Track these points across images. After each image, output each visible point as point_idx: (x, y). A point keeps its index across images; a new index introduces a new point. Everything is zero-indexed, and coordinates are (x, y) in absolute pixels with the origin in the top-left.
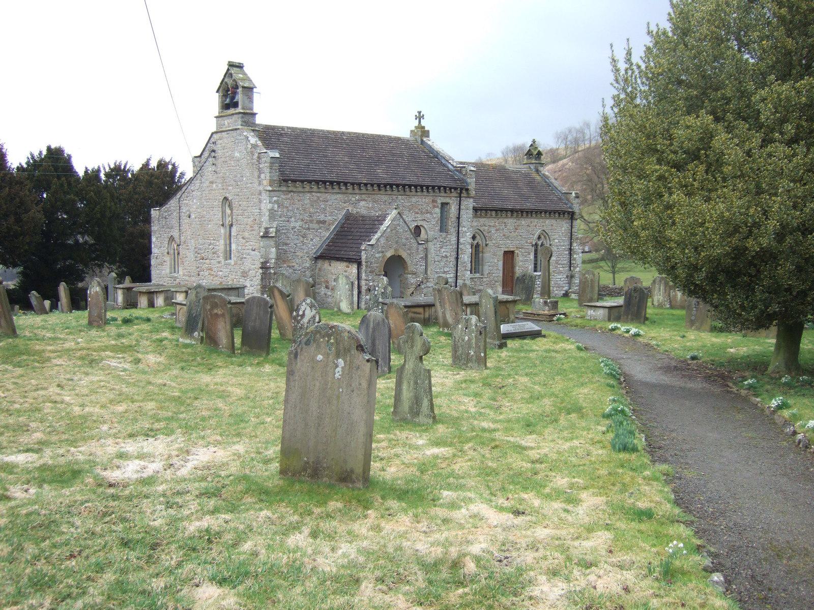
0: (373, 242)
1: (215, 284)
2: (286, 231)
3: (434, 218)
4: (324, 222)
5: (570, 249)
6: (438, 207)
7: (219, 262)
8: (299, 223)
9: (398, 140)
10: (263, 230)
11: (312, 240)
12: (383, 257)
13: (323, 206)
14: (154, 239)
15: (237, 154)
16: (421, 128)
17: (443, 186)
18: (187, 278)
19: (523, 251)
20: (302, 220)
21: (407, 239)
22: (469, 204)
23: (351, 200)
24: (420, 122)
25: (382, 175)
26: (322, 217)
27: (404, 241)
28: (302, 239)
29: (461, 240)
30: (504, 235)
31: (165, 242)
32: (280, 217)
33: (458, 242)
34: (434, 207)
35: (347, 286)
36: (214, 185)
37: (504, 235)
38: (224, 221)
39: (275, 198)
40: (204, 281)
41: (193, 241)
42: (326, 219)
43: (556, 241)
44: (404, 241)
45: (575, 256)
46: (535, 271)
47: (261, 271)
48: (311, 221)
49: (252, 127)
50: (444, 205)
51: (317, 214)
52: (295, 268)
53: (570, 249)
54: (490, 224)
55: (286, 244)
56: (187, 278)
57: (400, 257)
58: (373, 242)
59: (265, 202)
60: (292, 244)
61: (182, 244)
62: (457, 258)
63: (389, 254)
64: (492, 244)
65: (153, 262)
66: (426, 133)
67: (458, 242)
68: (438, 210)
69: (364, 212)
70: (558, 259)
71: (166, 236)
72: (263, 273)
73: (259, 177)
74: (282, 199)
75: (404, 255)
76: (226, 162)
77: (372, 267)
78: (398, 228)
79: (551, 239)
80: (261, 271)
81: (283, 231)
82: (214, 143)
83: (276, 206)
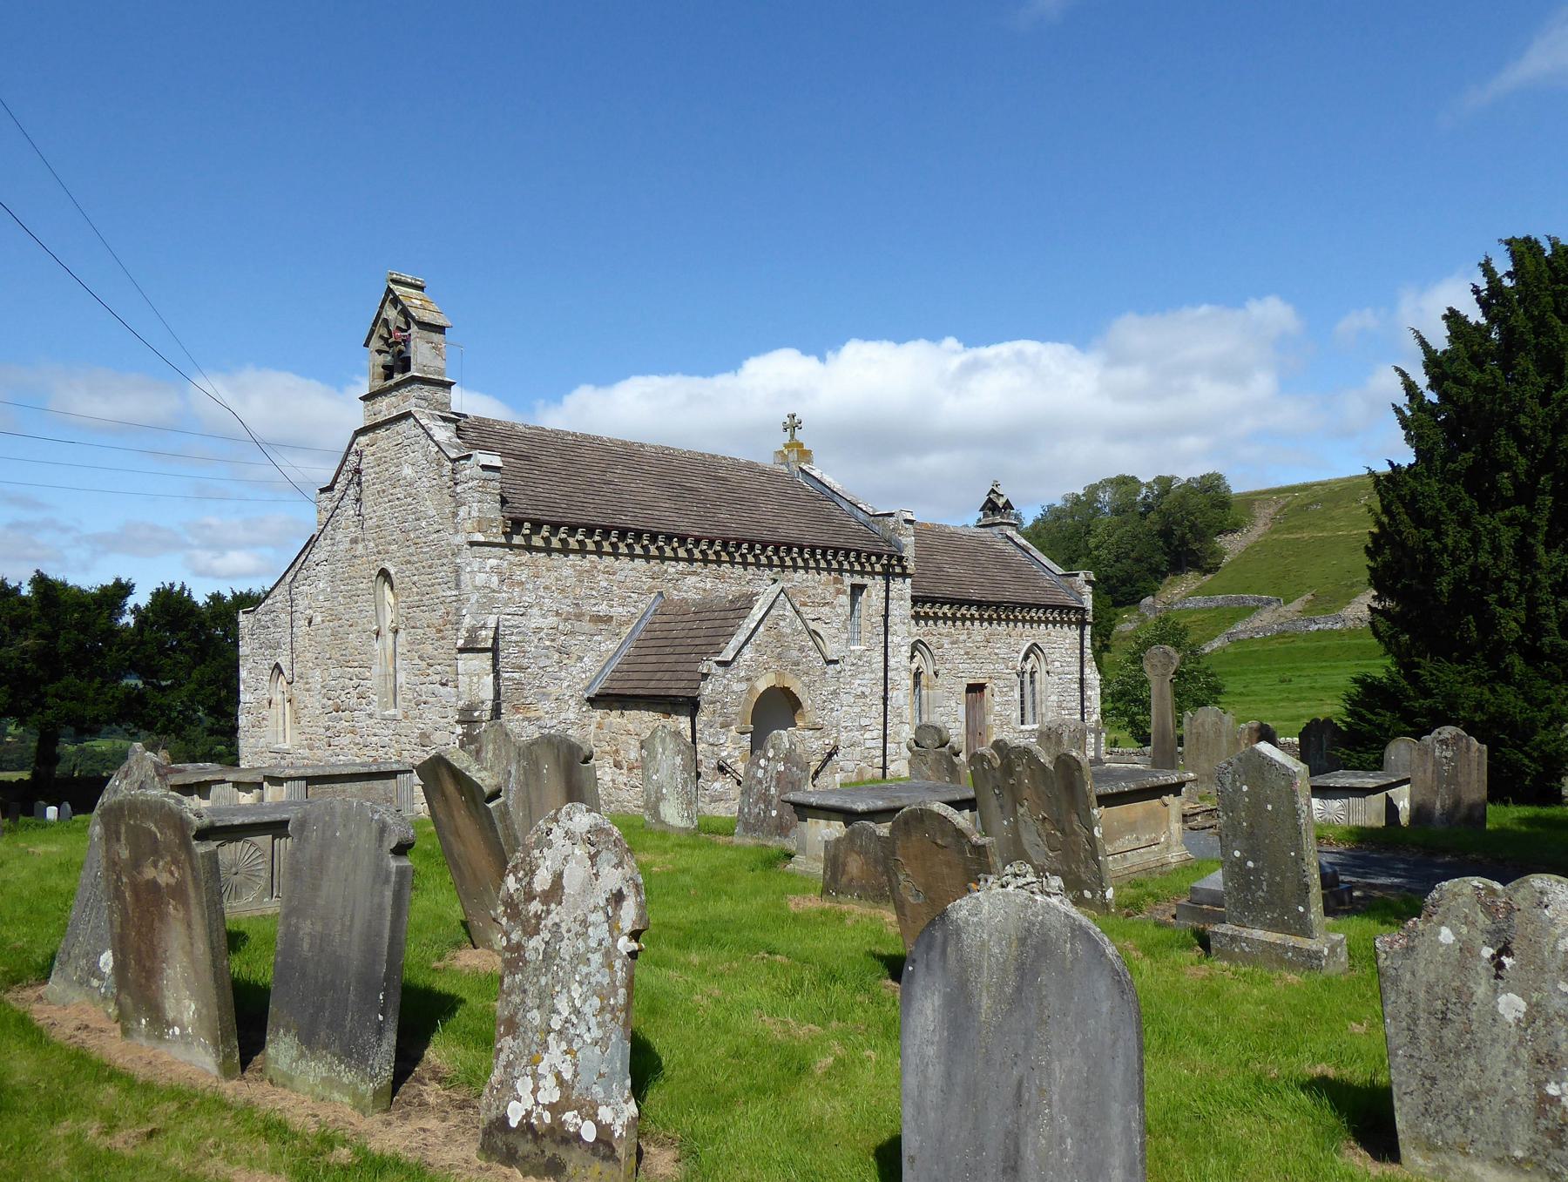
0: (728, 655)
1: (363, 765)
2: (519, 639)
3: (839, 615)
4: (608, 619)
5: (1082, 680)
6: (844, 592)
7: (370, 716)
8: (552, 620)
9: (751, 466)
10: (463, 633)
11: (580, 659)
12: (751, 690)
13: (604, 584)
14: (243, 674)
15: (408, 471)
16: (794, 445)
17: (854, 550)
18: (306, 752)
19: (1001, 683)
20: (557, 614)
21: (801, 649)
22: (903, 589)
23: (666, 571)
24: (792, 436)
25: (731, 521)
26: (603, 609)
27: (795, 653)
28: (556, 656)
29: (892, 662)
30: (967, 653)
31: (265, 678)
32: (506, 605)
33: (886, 666)
34: (839, 592)
35: (678, 760)
36: (360, 546)
37: (967, 653)
38: (381, 624)
39: (493, 562)
40: (341, 757)
41: (318, 672)
42: (614, 612)
43: (1057, 664)
44: (795, 653)
45: (1089, 693)
46: (1022, 723)
47: (459, 730)
48: (579, 617)
49: (442, 412)
50: (857, 590)
51: (593, 601)
52: (541, 723)
53: (1082, 680)
54: (940, 634)
55: (521, 668)
56: (306, 752)
57: (786, 693)
58: (728, 655)
59: (468, 569)
60: (533, 669)
61: (296, 679)
62: (885, 699)
63: (762, 685)
64: (946, 671)
65: (243, 721)
66: (805, 455)
67: (886, 666)
68: (845, 599)
69: (693, 595)
70: (1062, 698)
71: (266, 667)
72: (464, 735)
73: (455, 515)
74: (511, 563)
75: (797, 688)
76: (384, 491)
77: (725, 715)
78: (782, 623)
79: (1049, 660)
80: (459, 730)
81: (514, 638)
82: (360, 454)
83: (495, 579)
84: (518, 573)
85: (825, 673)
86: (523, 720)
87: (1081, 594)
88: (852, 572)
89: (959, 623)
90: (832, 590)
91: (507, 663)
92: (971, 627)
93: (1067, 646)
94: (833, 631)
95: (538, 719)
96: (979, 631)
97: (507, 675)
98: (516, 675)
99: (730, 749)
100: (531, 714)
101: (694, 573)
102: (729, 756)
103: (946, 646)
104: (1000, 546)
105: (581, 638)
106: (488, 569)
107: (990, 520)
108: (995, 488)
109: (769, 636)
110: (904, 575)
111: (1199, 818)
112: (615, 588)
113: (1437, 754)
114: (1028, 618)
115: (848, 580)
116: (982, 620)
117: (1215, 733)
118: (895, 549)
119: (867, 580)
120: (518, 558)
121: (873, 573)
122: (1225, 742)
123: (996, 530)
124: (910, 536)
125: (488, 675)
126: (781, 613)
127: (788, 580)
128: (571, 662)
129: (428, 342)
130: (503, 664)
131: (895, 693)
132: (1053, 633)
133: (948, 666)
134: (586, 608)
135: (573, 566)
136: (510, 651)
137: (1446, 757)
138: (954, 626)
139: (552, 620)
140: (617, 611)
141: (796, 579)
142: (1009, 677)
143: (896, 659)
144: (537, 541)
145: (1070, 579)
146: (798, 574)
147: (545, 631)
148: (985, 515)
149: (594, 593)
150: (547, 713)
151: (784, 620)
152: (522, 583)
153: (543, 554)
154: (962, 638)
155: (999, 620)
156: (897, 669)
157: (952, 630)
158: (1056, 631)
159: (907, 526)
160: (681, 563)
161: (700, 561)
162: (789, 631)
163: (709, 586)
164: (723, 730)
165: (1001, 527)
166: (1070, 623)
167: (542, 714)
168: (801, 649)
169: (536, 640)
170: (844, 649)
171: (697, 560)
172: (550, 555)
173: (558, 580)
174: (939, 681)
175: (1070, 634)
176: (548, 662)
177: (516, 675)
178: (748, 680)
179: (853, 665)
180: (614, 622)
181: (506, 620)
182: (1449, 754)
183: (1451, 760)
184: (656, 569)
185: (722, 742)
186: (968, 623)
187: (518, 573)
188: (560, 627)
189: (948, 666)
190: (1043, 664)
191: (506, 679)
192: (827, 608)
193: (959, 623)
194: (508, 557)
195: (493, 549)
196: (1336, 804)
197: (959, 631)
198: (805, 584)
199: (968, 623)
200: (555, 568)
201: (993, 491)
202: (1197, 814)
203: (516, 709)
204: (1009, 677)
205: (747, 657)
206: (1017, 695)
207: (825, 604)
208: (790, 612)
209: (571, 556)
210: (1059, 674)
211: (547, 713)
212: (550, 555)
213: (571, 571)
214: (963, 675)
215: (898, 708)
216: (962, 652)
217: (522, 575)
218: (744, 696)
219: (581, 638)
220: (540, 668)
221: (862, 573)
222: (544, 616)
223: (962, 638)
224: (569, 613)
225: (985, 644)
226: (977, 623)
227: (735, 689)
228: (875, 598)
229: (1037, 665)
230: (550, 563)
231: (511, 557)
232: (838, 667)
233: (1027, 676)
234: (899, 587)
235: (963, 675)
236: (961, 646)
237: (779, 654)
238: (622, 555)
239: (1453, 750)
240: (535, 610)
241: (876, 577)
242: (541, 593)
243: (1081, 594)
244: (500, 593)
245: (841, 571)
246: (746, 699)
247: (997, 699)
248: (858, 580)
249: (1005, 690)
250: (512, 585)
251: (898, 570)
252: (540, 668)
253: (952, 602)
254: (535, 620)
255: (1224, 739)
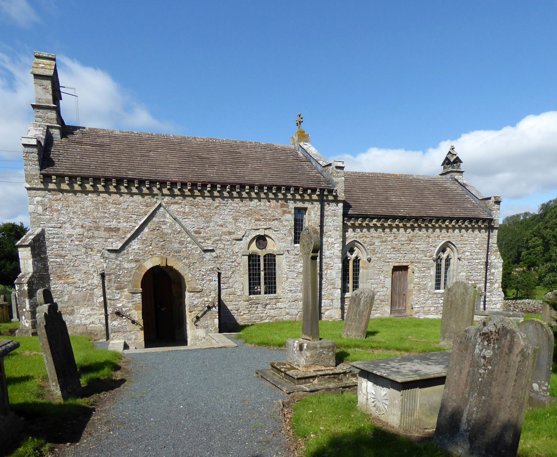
2: (58, 240)
3: (285, 226)
6: (290, 212)
8: (79, 230)
12: (139, 268)
13: (113, 210)
19: (420, 265)
20: (82, 227)
21: (181, 243)
26: (114, 224)
27: (176, 246)
28: (83, 250)
30: (394, 248)
34: (284, 212)
48: (97, 228)
49: (51, 123)
52: (77, 285)
53: (487, 263)
55: (61, 256)
63: (149, 265)
70: (469, 274)
74: (50, 199)
78: (163, 227)
81: (55, 240)
84: (56, 205)
85: (203, 258)
86: (64, 283)
87: (491, 210)
88: (295, 200)
89: (387, 230)
90: (280, 211)
91: (52, 253)
92: (397, 232)
93: (477, 243)
94: (280, 235)
95: (74, 283)
96: (403, 235)
97: (52, 260)
98: (58, 260)
99: (124, 302)
100: (70, 281)
101: (176, 203)
102: (123, 306)
103: (376, 244)
104: (448, 185)
105: (99, 240)
106: (35, 203)
107: (446, 171)
108: (451, 151)
109: (153, 234)
110: (336, 200)
111: (316, 381)
112: (121, 212)
113: (477, 351)
114: (457, 226)
115: (292, 205)
116: (405, 228)
117: (462, 301)
118: (331, 185)
119: (307, 205)
120: (55, 197)
121: (311, 201)
122: (467, 308)
123: (448, 176)
124: (341, 177)
125: (30, 259)
126: (162, 220)
127: (246, 206)
128: (94, 253)
129: (40, 86)
130: (49, 254)
131: (329, 271)
132: (465, 235)
133: (378, 255)
134: (101, 224)
135: (92, 200)
136: (53, 247)
137: (484, 357)
138: (384, 231)
139: (79, 230)
140: (123, 225)
141: (251, 205)
142: (427, 261)
143: (330, 252)
144: (64, 186)
145: (487, 201)
146: (253, 202)
147: (75, 236)
148: (445, 168)
149: (106, 215)
150: (80, 280)
151: (165, 224)
152: (58, 210)
153: (71, 194)
154: (389, 239)
155: (420, 228)
156: (331, 257)
157: (382, 234)
158: (468, 235)
159: (338, 170)
160: (167, 198)
161: (180, 195)
162: (170, 231)
163: (187, 210)
164: (117, 291)
165: (451, 174)
166: (480, 228)
167: (76, 280)
168: (181, 243)
169: (69, 241)
170: (289, 245)
171: (177, 195)
172: (75, 194)
173: (81, 208)
174: (371, 264)
175: (479, 235)
176: (78, 253)
177: (58, 260)
178: (136, 261)
179: (296, 255)
180: (121, 231)
181: (49, 230)
182: (488, 353)
183: (489, 361)
184: (149, 201)
185: (117, 298)
186: (395, 230)
187: (56, 205)
188: (85, 234)
189: (378, 255)
190: (456, 254)
191: (52, 262)
192: (276, 222)
193: (387, 230)
194: (48, 196)
195: (38, 192)
196: (384, 391)
197: (388, 235)
198: (258, 208)
199: (395, 230)
200: (80, 202)
201: (450, 153)
202: (314, 377)
203: (60, 278)
204: (427, 261)
205: (136, 247)
206: (433, 272)
207: (274, 220)
208: (169, 219)
209: (90, 195)
210: (468, 259)
211: (80, 280)
212: (75, 194)
213: (89, 203)
214: (390, 260)
215: (331, 280)
216: (390, 247)
217: (58, 206)
218: (134, 271)
219: (99, 240)
220: (74, 256)
221: (303, 200)
222: (73, 228)
223: (389, 239)
224: (90, 226)
225: (409, 242)
226: (402, 230)
227: (126, 267)
228: (313, 216)
229: (452, 254)
230: (76, 199)
231: (49, 195)
232: (214, 254)
233: (443, 262)
234: (333, 208)
235: (390, 260)
236: (389, 243)
237: (162, 246)
238: (124, 193)
239: (494, 349)
240: (67, 225)
241: (314, 203)
242: (71, 215)
243: (491, 210)
244: (44, 215)
245: (286, 199)
246: (136, 273)
247: (416, 275)
248: (300, 205)
249: (423, 269)
250: (52, 211)
251: (331, 198)
252: (74, 256)
253: (379, 218)
254: (68, 230)
255: (467, 306)
